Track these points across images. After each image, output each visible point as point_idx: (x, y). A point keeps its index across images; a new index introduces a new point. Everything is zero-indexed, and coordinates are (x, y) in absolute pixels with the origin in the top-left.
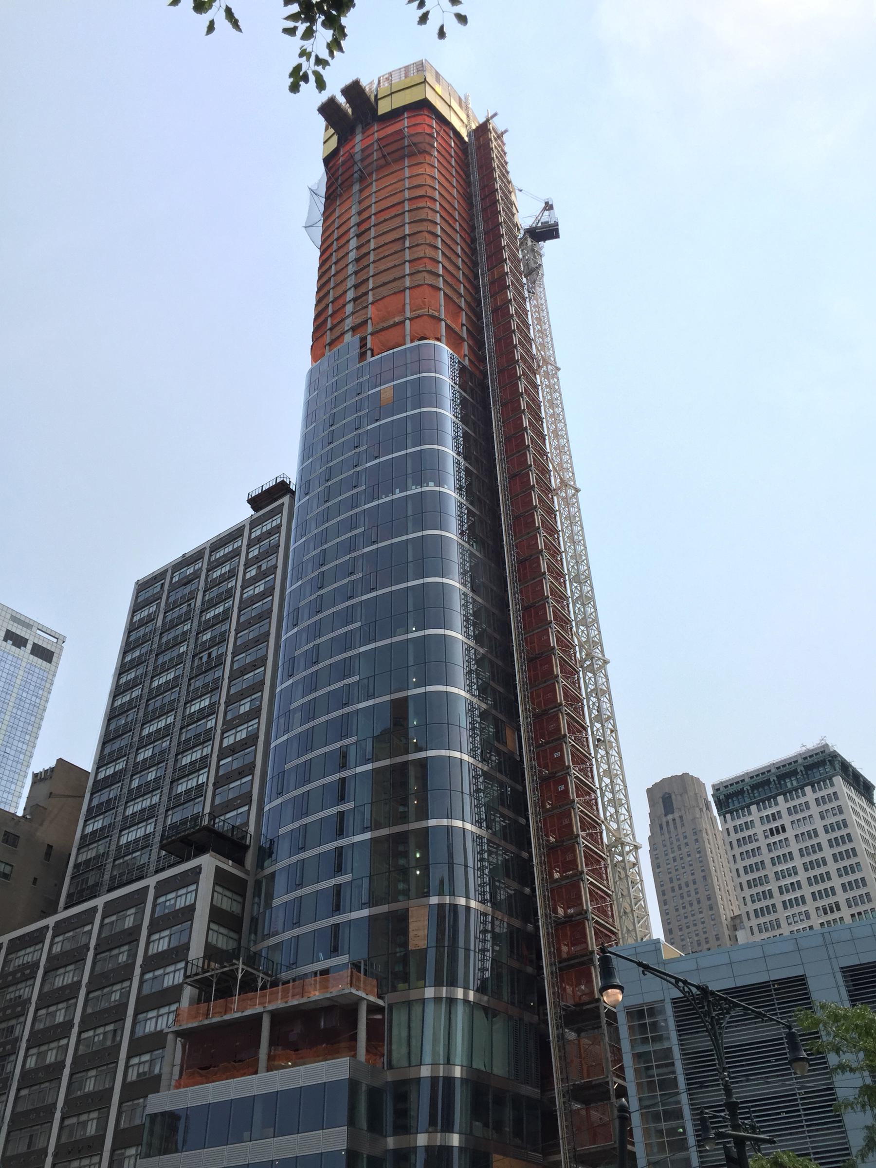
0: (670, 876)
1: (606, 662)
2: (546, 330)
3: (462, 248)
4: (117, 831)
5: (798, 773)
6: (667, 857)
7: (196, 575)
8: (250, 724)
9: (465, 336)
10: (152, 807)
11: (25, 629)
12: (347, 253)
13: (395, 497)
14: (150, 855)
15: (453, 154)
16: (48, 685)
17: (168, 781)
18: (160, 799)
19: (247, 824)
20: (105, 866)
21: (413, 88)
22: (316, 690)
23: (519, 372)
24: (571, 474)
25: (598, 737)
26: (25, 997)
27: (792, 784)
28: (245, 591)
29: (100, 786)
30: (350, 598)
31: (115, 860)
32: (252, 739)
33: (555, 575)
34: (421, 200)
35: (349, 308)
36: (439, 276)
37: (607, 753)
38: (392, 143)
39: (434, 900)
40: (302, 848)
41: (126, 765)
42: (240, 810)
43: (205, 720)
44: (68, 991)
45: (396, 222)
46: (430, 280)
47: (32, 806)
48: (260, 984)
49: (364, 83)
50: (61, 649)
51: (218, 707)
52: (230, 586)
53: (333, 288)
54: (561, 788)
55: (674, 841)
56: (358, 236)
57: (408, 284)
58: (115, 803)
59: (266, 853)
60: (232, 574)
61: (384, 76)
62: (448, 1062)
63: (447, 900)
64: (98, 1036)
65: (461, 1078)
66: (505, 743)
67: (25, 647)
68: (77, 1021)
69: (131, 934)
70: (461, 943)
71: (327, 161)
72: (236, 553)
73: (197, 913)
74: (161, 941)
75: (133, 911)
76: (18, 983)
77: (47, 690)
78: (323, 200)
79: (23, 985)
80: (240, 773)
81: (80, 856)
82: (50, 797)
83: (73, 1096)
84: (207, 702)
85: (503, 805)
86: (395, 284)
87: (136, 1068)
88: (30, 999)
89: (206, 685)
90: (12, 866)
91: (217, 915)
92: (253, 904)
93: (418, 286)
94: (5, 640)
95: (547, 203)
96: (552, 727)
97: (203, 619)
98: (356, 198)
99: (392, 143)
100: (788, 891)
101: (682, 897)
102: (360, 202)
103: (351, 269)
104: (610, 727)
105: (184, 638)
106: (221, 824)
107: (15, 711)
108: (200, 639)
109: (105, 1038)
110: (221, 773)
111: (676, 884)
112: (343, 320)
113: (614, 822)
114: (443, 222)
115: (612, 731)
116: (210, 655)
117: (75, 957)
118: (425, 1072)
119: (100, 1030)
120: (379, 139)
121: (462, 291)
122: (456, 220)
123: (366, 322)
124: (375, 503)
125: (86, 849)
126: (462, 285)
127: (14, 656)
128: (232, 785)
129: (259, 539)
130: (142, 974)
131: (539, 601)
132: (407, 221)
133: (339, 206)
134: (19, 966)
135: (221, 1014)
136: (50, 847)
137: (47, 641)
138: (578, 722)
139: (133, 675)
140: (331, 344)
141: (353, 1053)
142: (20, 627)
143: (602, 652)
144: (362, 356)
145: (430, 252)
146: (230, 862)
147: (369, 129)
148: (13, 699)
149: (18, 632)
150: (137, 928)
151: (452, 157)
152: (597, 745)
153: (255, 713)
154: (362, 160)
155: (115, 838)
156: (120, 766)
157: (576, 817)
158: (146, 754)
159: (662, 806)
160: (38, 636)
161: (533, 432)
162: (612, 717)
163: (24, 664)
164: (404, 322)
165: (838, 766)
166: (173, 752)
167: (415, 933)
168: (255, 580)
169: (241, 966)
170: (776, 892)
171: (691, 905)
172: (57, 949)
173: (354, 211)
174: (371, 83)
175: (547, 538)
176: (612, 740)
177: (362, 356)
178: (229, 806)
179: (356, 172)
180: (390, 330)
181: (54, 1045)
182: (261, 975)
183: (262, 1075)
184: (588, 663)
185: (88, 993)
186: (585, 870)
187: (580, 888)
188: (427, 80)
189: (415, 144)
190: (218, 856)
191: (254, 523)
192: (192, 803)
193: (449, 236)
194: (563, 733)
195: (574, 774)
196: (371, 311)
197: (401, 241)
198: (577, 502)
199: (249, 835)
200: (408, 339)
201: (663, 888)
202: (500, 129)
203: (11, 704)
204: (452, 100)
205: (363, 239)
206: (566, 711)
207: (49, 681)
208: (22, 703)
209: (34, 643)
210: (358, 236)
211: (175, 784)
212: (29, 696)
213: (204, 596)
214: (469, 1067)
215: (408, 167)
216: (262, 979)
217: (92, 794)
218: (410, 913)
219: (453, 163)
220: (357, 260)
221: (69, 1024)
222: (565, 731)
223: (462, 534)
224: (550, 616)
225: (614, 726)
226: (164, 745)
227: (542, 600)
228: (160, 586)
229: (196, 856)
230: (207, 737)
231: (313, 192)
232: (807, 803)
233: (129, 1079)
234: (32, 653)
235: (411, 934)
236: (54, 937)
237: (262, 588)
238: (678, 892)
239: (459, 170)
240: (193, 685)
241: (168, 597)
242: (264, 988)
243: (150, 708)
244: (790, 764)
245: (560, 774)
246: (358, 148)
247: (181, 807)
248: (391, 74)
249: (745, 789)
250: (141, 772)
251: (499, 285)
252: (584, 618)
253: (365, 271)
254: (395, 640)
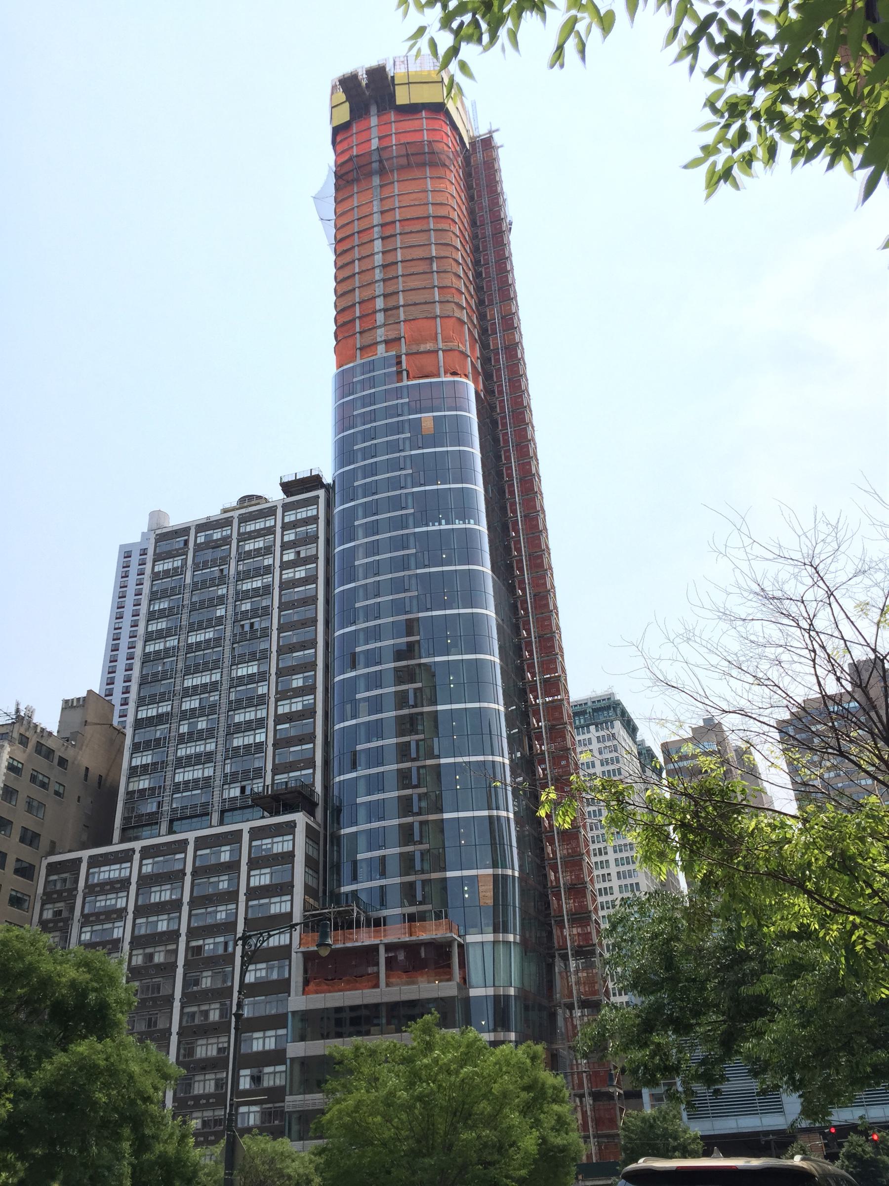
34: (443, 220)
35: (380, 318)
91: (310, 863)
105: (222, 600)
129: (294, 525)
158: (193, 703)
165: (619, 712)
232: (590, 739)
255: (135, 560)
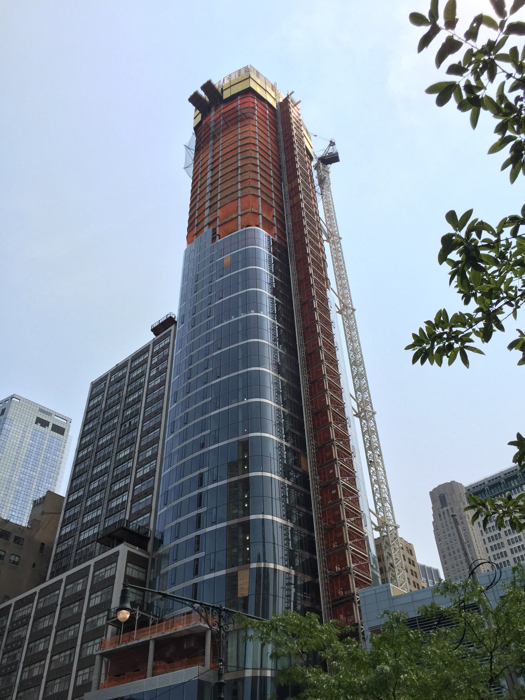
0: (447, 546)
1: (374, 413)
2: (332, 216)
3: (273, 172)
4: (78, 533)
5: (518, 477)
6: (445, 534)
7: (124, 377)
8: (152, 463)
9: (275, 222)
10: (97, 517)
11: (47, 416)
12: (206, 181)
13: (231, 321)
14: (96, 546)
15: (268, 118)
16: (62, 448)
17: (106, 500)
18: (102, 512)
19: (149, 524)
20: (71, 554)
21: (243, 82)
22: (186, 440)
23: (307, 241)
24: (349, 301)
25: (370, 460)
26: (23, 636)
27: (515, 484)
28: (150, 384)
29: (70, 505)
30: (206, 383)
31: (77, 551)
32: (152, 473)
33: (330, 361)
34: (247, 146)
35: (207, 212)
36: (258, 189)
37: (376, 469)
38: (230, 115)
39: (254, 565)
40: (177, 537)
41: (84, 492)
42: (145, 516)
43: (127, 463)
44: (46, 631)
45: (234, 160)
46: (252, 191)
47: (33, 521)
48: (151, 623)
49: (215, 82)
50: (69, 427)
51: (134, 454)
52: (141, 381)
53: (198, 202)
54: (334, 492)
55: (449, 524)
56: (212, 170)
57: (239, 195)
58: (77, 516)
59: (159, 542)
60: (143, 374)
61: (226, 77)
62: (262, 668)
63: (262, 565)
64: (61, 658)
65: (271, 677)
66: (300, 466)
67: (48, 426)
68: (50, 649)
69: (80, 595)
70: (271, 592)
71: (196, 128)
72: (145, 362)
73: (116, 580)
74: (97, 598)
75: (81, 581)
76: (19, 628)
77: (62, 451)
78: (194, 152)
79: (21, 629)
80: (145, 494)
81: (58, 549)
82: (42, 514)
83: (47, 696)
84: (128, 452)
85: (299, 504)
86: (232, 196)
87: (81, 677)
88: (25, 637)
89: (127, 442)
90: (20, 557)
92: (151, 573)
93: (246, 195)
94: (36, 423)
95: (331, 142)
96: (328, 454)
97: (127, 402)
98: (211, 148)
99: (230, 115)
100: (516, 552)
101: (456, 559)
102: (213, 151)
103: (208, 189)
104: (378, 453)
106: (133, 526)
107: (43, 465)
108: (125, 414)
109: (65, 660)
110: (135, 494)
111: (451, 551)
112: (204, 219)
113: (382, 512)
114: (261, 158)
115: (379, 456)
116: (130, 423)
117: (50, 610)
118: (248, 673)
119: (62, 655)
120: (224, 113)
121: (273, 197)
122: (270, 156)
123: (216, 219)
124: (220, 325)
125: (61, 545)
126: (273, 193)
127: (41, 432)
128: (141, 501)
129: (158, 352)
130: (86, 619)
131: (320, 378)
132: (239, 158)
133: (202, 154)
134: (20, 617)
135: (126, 642)
136: (43, 544)
137: (60, 423)
138: (345, 451)
139: (88, 438)
140: (197, 234)
141: (203, 663)
142: (45, 415)
143: (372, 407)
144: (214, 239)
145: (252, 175)
146: (137, 548)
147: (218, 108)
148: (42, 458)
149: (44, 418)
150: (84, 591)
151: (267, 119)
152: (370, 465)
153: (154, 457)
154: (215, 126)
155: (77, 537)
156: (81, 493)
157: (343, 510)
159: (439, 501)
160: (61, 422)
161: (316, 276)
162: (379, 447)
163: (47, 437)
164: (237, 217)
166: (110, 482)
167: (242, 586)
168: (155, 377)
169: (138, 612)
170: (509, 553)
171: (462, 563)
172: (41, 605)
173: (209, 156)
174: (220, 82)
175: (324, 339)
176: (379, 461)
177: (214, 239)
178: (139, 514)
179: (211, 134)
180: (230, 223)
181: (37, 664)
182: (152, 617)
183: (149, 678)
184: (363, 414)
185: (56, 632)
186: (349, 542)
187: (345, 553)
188: (251, 76)
189: (243, 114)
190: (129, 544)
191: (155, 343)
192: (119, 513)
193: (265, 165)
194: (334, 458)
195: (342, 483)
196: (219, 213)
197: (236, 171)
198: (354, 317)
199: (150, 531)
200: (240, 227)
201: (444, 554)
202: (296, 101)
203: (41, 461)
204: (267, 86)
205: (215, 171)
206: (336, 444)
207: (63, 446)
208: (47, 460)
209: (53, 424)
210: (212, 170)
211: (110, 502)
212: (51, 456)
213: (127, 388)
214: (275, 669)
215: (240, 127)
216: (153, 619)
217: (65, 511)
218: (238, 574)
219: (268, 123)
220: (211, 184)
221: (46, 651)
222: (336, 456)
223: (275, 340)
224: (326, 386)
225: (380, 452)
226: (105, 479)
227: (322, 377)
228: (104, 385)
229: (117, 545)
230: (127, 473)
231: (187, 147)
233: (77, 684)
234: (52, 430)
235: (239, 587)
236: (39, 598)
237: (159, 381)
238: (453, 556)
239: (272, 127)
240: (121, 442)
241: (108, 391)
242: (153, 624)
243: (98, 457)
244: (512, 471)
245: (333, 483)
246: (212, 119)
247: (113, 516)
248: (230, 75)
249: (486, 489)
250: (92, 496)
251: (295, 191)
252: (360, 387)
253: (216, 189)
254: (230, 406)
255: (203, 573)
